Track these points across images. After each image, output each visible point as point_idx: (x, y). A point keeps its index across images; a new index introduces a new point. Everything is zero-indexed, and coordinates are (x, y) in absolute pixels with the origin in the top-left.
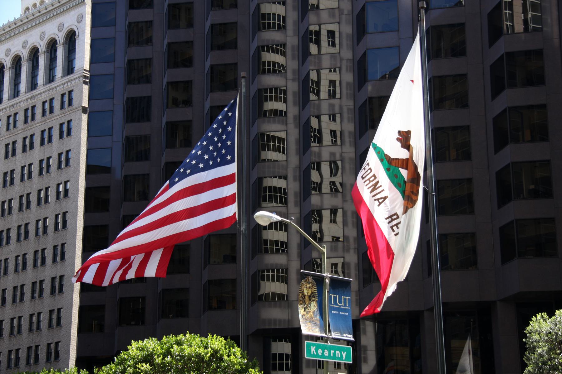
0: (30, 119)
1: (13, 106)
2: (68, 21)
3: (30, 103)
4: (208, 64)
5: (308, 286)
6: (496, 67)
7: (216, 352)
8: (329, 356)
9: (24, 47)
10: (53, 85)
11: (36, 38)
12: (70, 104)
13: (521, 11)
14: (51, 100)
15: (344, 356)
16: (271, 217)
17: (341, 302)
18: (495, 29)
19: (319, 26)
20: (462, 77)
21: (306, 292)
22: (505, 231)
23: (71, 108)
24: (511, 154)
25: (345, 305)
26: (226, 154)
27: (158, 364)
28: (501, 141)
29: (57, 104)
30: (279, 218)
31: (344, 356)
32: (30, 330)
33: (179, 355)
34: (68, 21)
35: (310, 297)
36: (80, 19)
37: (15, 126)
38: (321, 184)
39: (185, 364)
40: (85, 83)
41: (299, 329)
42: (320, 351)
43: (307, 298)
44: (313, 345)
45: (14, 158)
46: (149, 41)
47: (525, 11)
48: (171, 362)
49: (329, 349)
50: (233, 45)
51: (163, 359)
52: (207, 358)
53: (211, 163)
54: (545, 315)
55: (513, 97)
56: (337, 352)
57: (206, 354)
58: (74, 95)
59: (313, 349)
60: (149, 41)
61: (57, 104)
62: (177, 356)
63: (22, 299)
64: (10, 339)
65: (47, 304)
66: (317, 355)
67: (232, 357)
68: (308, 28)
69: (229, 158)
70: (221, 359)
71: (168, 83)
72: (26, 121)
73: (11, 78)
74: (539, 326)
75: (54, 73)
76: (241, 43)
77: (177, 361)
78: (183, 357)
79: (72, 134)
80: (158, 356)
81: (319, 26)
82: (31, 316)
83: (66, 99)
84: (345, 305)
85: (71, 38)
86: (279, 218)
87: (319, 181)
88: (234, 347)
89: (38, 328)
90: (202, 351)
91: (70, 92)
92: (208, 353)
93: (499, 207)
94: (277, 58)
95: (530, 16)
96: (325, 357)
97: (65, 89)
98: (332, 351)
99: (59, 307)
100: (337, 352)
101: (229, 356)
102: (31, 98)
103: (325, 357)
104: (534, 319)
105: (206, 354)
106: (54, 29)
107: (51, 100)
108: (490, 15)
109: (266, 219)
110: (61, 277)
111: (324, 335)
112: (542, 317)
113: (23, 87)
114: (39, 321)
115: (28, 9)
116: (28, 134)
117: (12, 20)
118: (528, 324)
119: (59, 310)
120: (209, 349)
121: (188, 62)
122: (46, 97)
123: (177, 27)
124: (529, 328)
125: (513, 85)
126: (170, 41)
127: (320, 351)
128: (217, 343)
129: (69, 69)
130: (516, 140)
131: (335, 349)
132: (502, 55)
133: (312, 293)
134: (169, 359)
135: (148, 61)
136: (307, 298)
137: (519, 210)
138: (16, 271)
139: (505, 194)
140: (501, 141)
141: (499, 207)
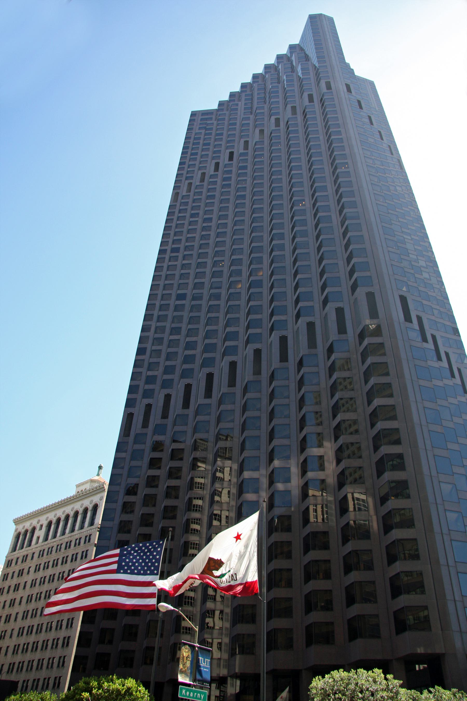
0: (68, 547)
1: (61, 540)
2: (95, 499)
3: (70, 539)
4: (160, 526)
5: (186, 651)
6: (306, 539)
7: (129, 689)
8: (193, 697)
9: (72, 510)
10: (82, 531)
11: (78, 507)
12: (89, 541)
13: (321, 514)
14: (80, 538)
15: (202, 697)
16: (167, 607)
17: (204, 662)
18: (306, 521)
19: (221, 511)
20: (289, 543)
21: (185, 654)
22: (308, 628)
23: (89, 543)
24: (313, 585)
25: (207, 665)
26: (154, 570)
27: (93, 694)
28: (308, 577)
29: (82, 541)
30: (172, 608)
31: (202, 697)
32: (47, 667)
33: (107, 689)
34: (95, 499)
35: (187, 657)
36: (101, 499)
37: (60, 551)
38: (215, 596)
39: (110, 695)
40: (98, 531)
41: (178, 679)
42: (188, 693)
43: (185, 658)
44: (184, 689)
45: (56, 568)
46: (132, 512)
47: (323, 515)
48: (102, 694)
49: (194, 692)
50: (174, 517)
51: (98, 691)
52: (123, 692)
53: (142, 572)
54: (320, 677)
55: (314, 555)
56: (199, 694)
57: (123, 690)
58: (92, 537)
59: (184, 691)
60: (132, 512)
61: (82, 541)
62: (105, 689)
63: (46, 648)
64: (36, 672)
65: (59, 652)
66: (186, 696)
67: (138, 693)
68: (213, 512)
69: (156, 572)
70: (131, 694)
71: (139, 534)
72: (66, 548)
73: (63, 526)
74: (317, 685)
75: (84, 525)
76: (178, 516)
77: (105, 693)
78: (108, 690)
79: (88, 557)
80: (95, 689)
81: (221, 511)
82: (49, 659)
83: (88, 539)
84: (207, 665)
85: (96, 507)
86: (172, 608)
87: (214, 594)
88: (140, 687)
89: (52, 667)
90: (120, 687)
91: (90, 535)
92: (124, 689)
93: (306, 614)
94: (197, 527)
95: (325, 516)
96: (191, 697)
97: (89, 533)
98: (195, 694)
99: (65, 655)
100: (199, 694)
101: (136, 692)
102: (70, 537)
103: (191, 697)
104: (314, 679)
105: (123, 690)
106: (88, 503)
107: (80, 538)
108: (304, 512)
109: (165, 608)
110: (69, 637)
111: (192, 683)
112: (319, 679)
113: (68, 530)
114: (53, 663)
115: (78, 492)
116: (66, 555)
117: (69, 496)
118: (311, 683)
119: (65, 657)
120: (125, 687)
121: (150, 525)
122: (78, 537)
123: (147, 506)
124: (311, 685)
125: (314, 549)
126: (143, 512)
127: (188, 693)
128: (131, 683)
129: (92, 523)
130: (315, 578)
131: (198, 692)
132: (309, 533)
133: (188, 655)
134: (100, 691)
135: (130, 522)
136: (185, 658)
137: (317, 616)
138: (46, 631)
139: (309, 606)
140: (308, 577)
141: (306, 614)
